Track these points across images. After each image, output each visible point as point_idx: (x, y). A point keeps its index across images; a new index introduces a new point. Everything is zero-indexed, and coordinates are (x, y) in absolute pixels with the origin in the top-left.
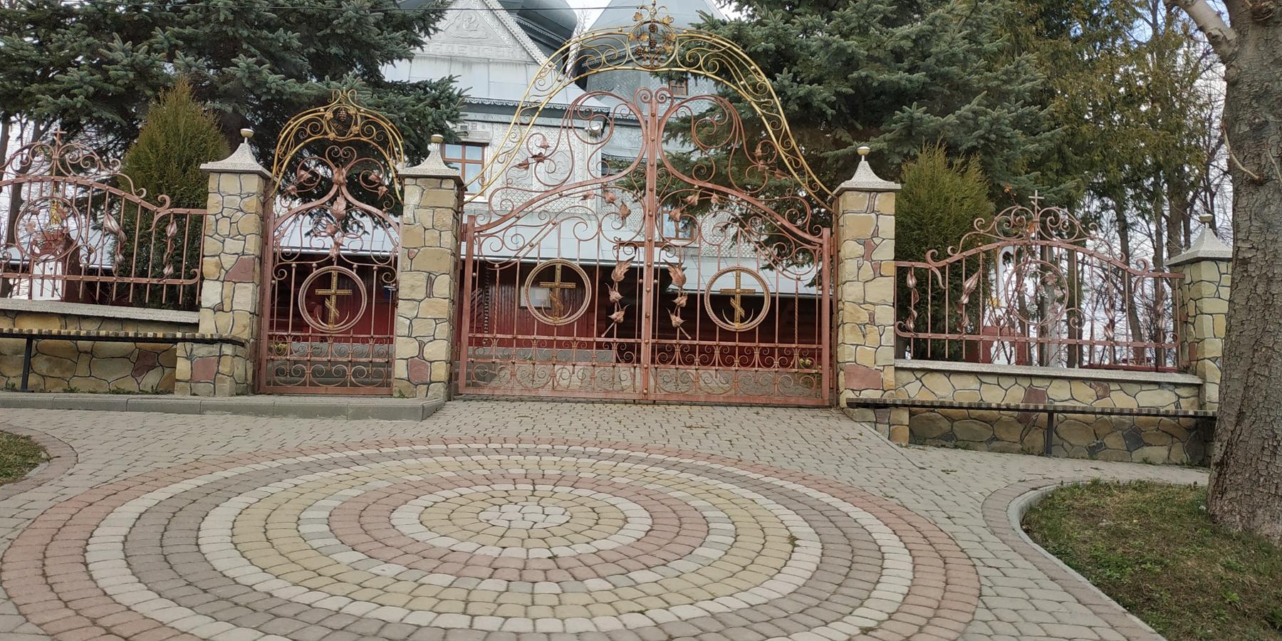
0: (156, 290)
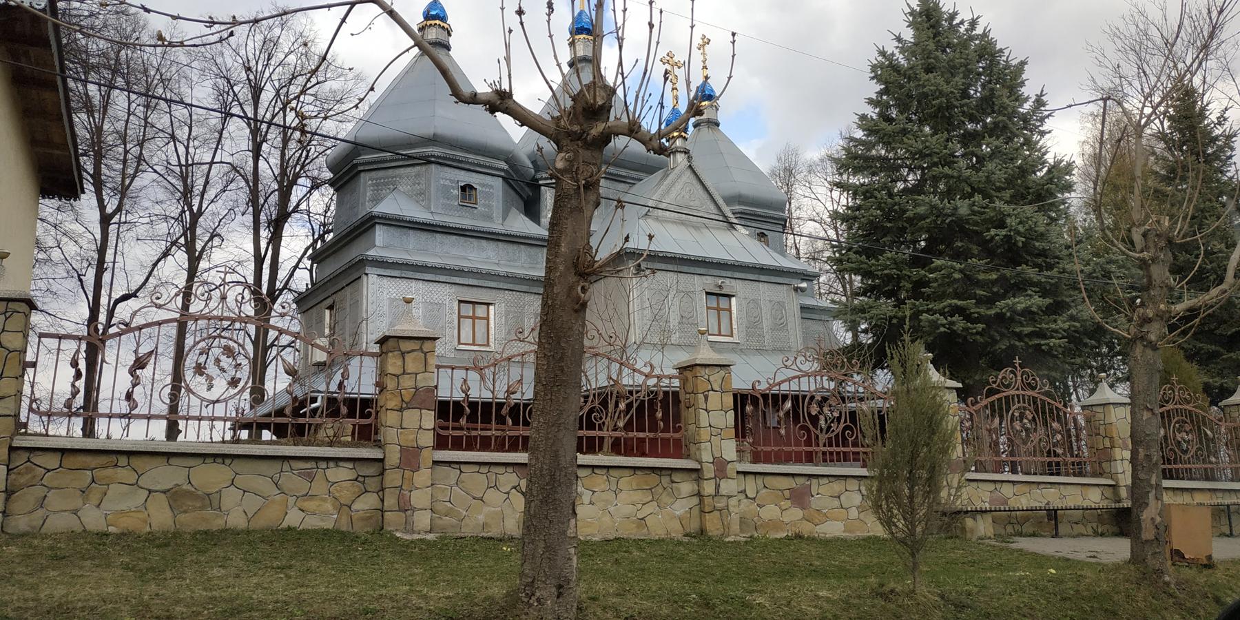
0: (653, 441)
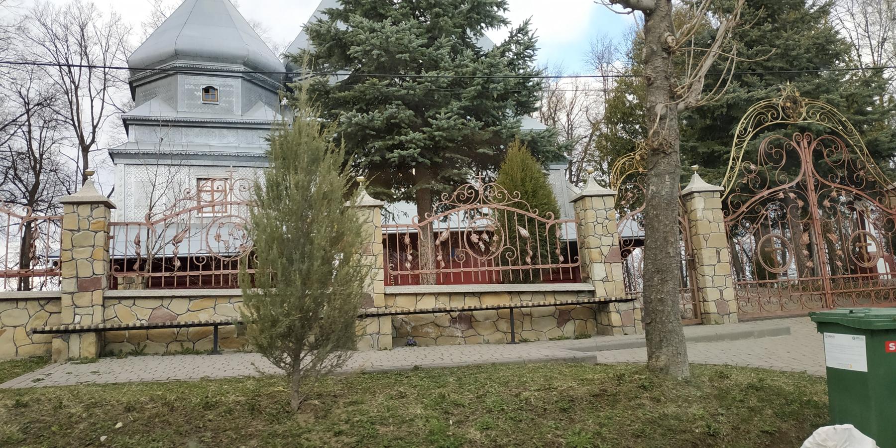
0: (556, 272)
